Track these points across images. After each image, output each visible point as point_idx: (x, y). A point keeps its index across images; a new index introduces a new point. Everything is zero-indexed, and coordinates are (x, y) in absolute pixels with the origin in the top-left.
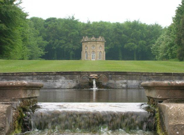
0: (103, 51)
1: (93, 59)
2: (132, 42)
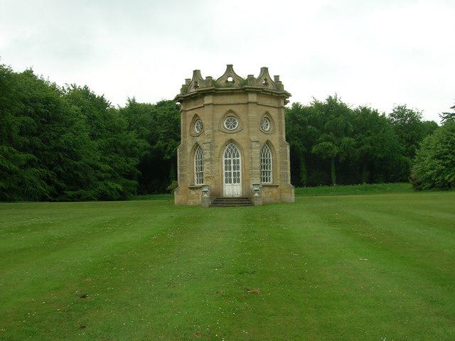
0: (281, 139)
1: (229, 181)
2: (328, 140)
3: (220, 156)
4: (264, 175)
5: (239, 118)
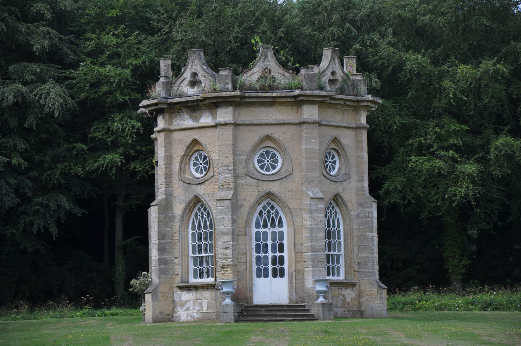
0: (359, 190)
1: (262, 273)
3: (247, 225)
4: (330, 263)
5: (283, 151)
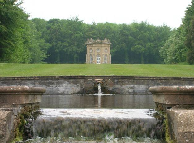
0: (109, 54)
1: (98, 62)
2: (139, 44)
